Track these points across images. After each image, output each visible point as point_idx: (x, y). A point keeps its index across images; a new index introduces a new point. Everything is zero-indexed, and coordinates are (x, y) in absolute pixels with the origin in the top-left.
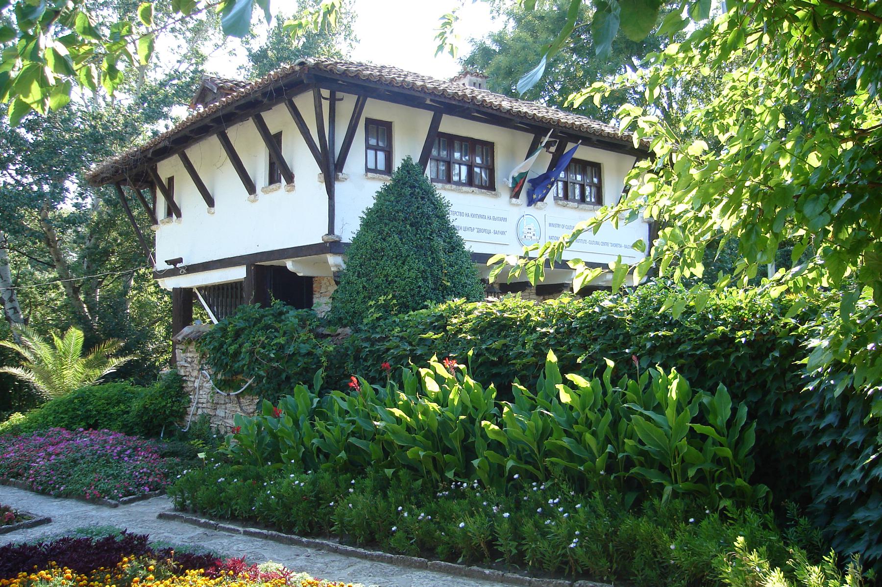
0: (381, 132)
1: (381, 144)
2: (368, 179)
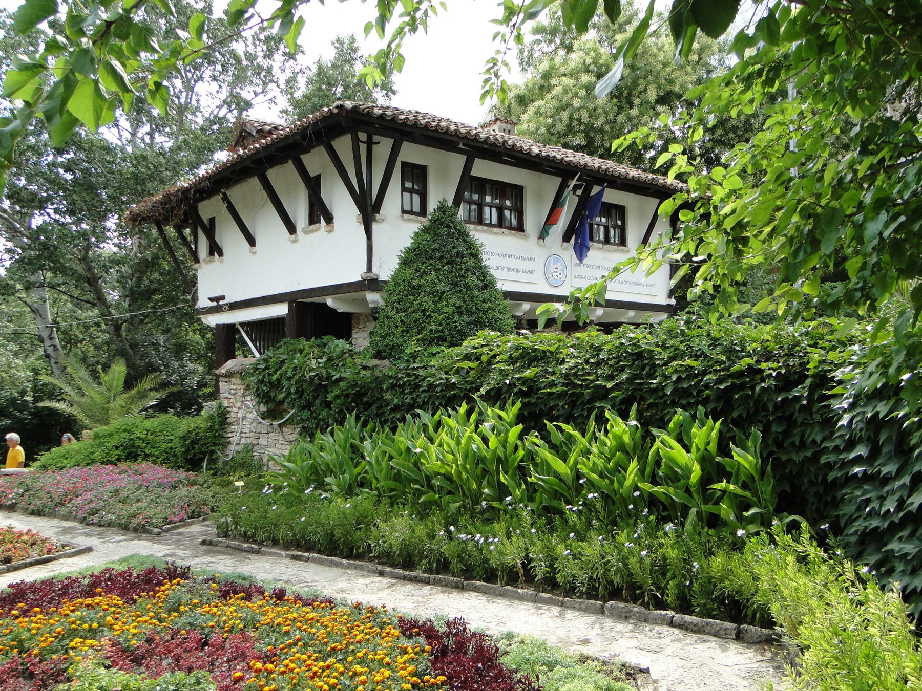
0: (416, 177)
1: (416, 187)
2: (405, 220)
